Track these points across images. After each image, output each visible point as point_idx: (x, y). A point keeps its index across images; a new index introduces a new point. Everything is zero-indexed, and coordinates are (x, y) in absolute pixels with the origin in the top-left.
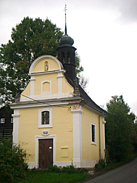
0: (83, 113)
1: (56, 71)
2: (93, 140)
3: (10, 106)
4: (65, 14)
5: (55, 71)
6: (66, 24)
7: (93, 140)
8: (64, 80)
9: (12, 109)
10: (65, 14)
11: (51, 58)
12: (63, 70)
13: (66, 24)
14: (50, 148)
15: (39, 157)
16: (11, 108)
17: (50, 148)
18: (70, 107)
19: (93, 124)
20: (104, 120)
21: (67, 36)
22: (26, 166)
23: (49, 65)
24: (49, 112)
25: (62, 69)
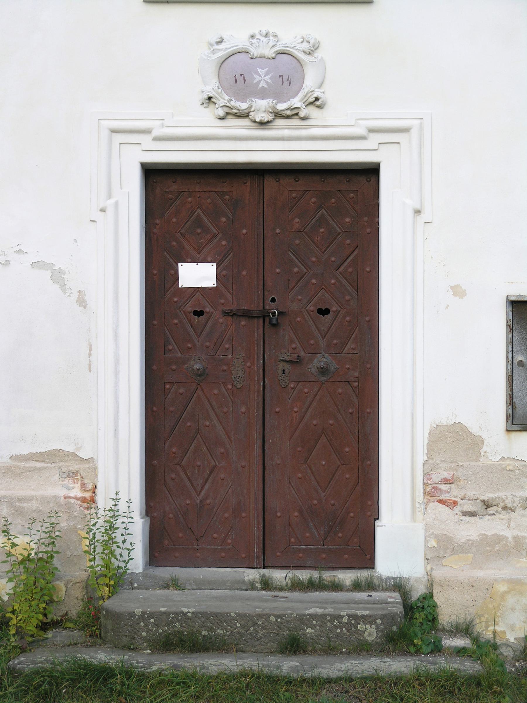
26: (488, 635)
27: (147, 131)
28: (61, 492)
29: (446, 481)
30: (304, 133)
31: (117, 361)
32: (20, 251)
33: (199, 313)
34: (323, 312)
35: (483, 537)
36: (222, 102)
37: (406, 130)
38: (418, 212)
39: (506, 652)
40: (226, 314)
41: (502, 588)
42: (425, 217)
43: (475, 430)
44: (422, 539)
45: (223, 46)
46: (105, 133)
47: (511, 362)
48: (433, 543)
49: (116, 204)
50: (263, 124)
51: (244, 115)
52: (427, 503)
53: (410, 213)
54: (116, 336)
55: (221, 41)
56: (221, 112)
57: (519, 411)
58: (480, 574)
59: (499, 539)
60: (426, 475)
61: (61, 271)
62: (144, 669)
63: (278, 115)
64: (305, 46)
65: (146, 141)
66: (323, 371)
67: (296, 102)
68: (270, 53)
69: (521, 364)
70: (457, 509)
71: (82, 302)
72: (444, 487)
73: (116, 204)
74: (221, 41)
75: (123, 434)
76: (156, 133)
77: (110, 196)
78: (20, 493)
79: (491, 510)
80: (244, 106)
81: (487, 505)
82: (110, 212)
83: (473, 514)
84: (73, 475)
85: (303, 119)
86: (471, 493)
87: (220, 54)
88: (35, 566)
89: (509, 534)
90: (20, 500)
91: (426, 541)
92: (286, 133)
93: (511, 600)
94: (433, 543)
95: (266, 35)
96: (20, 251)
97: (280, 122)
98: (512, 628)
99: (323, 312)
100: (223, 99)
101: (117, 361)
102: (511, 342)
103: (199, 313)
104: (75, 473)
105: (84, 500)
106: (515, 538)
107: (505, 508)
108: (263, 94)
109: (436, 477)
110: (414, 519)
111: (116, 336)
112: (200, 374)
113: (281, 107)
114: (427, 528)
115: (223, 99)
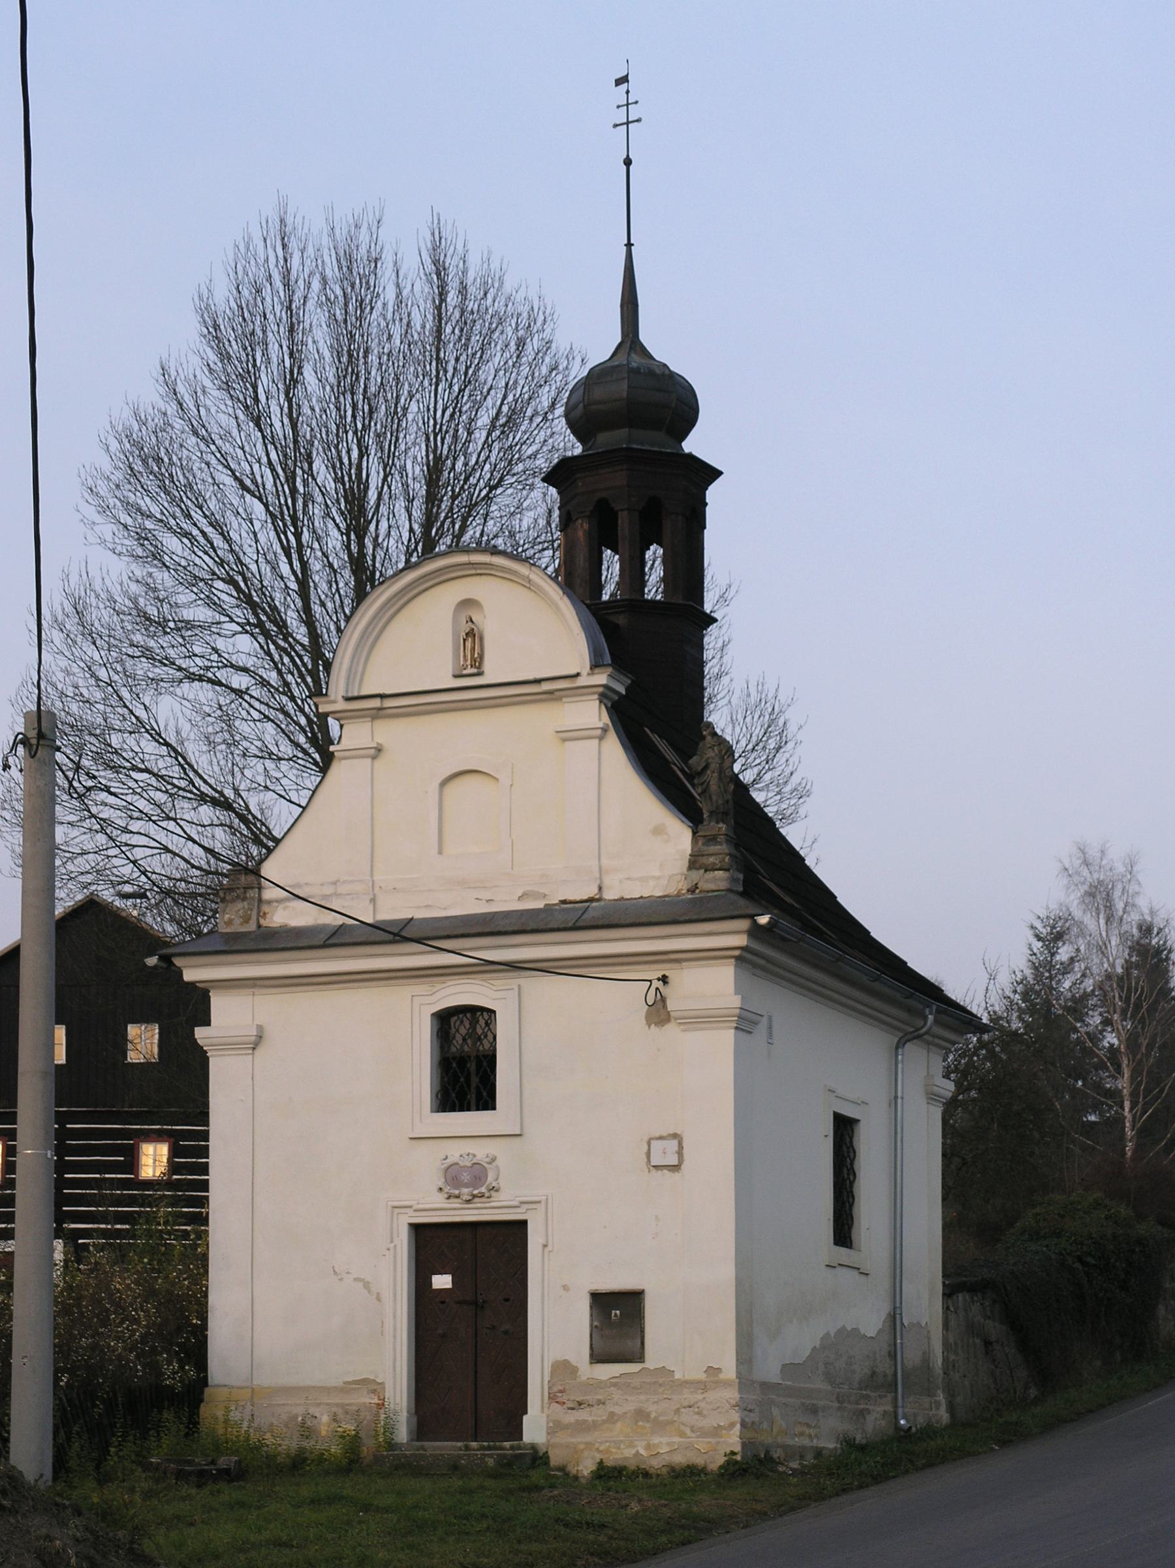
0: (765, 1020)
1: (546, 686)
2: (843, 1233)
3: (178, 962)
4: (628, 162)
5: (538, 681)
6: (629, 245)
7: (843, 1233)
8: (614, 751)
9: (192, 984)
10: (628, 162)
11: (510, 571)
12: (601, 678)
13: (629, 245)
14: (442, 1281)
15: (417, 1315)
16: (189, 976)
17: (442, 1281)
18: (664, 979)
19: (848, 1111)
20: (938, 1066)
21: (636, 361)
22: (693, 858)
23: (490, 626)
24: (494, 1012)
25: (596, 665)
26: (574, 1472)
27: (411, 1207)
28: (368, 1400)
29: (561, 1392)
30: (487, 1205)
31: (395, 1329)
32: (348, 1273)
33: (443, 1302)
34: (507, 1300)
35: (577, 1421)
36: (446, 1190)
37: (539, 1202)
38: (545, 1246)
39: (583, 1481)
40: (457, 1302)
41: (582, 1447)
42: (549, 1248)
43: (574, 1364)
44: (545, 1424)
45: (448, 1161)
46: (390, 1208)
47: (591, 1325)
48: (551, 1424)
49: (395, 1246)
50: (468, 1201)
51: (458, 1197)
52: (550, 1404)
53: (540, 1248)
54: (395, 1317)
55: (446, 1158)
56: (446, 1196)
57: (595, 1353)
58: (574, 1440)
59: (585, 1421)
60: (549, 1388)
61: (369, 1283)
62: (76, 636)
63: (474, 1196)
64: (488, 1160)
65: (410, 1212)
66: (506, 1332)
67: (483, 1190)
68: (469, 1164)
69: (596, 1327)
70: (565, 1406)
71: (379, 1299)
72: (560, 1395)
73: (395, 1246)
74: (446, 1158)
75: (398, 1369)
76: (415, 1207)
77: (392, 1242)
78: (348, 1402)
79: (582, 1407)
80: (457, 1192)
81: (580, 1404)
82: (392, 1251)
83: (573, 1409)
84: (374, 1391)
85: (488, 1197)
86: (572, 1398)
87: (445, 1165)
88: (225, 259)
89: (590, 1419)
90: (348, 1405)
91: (548, 1423)
92: (479, 1205)
93: (586, 1453)
94: (551, 1424)
95: (468, 1155)
96: (348, 1273)
97: (477, 1200)
98: (586, 1468)
99: (507, 1300)
100: (446, 1190)
101: (395, 1329)
102: (591, 1315)
103: (443, 1302)
104: (375, 1390)
105: (378, 1404)
106: (593, 1421)
107: (589, 1405)
108: (466, 1185)
109: (555, 1389)
110: (543, 1411)
111: (395, 1317)
112: (444, 1336)
113: (476, 1192)
114: (548, 1416)
115: (447, 1189)
